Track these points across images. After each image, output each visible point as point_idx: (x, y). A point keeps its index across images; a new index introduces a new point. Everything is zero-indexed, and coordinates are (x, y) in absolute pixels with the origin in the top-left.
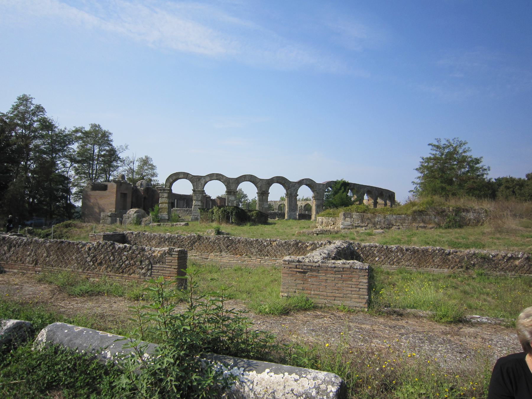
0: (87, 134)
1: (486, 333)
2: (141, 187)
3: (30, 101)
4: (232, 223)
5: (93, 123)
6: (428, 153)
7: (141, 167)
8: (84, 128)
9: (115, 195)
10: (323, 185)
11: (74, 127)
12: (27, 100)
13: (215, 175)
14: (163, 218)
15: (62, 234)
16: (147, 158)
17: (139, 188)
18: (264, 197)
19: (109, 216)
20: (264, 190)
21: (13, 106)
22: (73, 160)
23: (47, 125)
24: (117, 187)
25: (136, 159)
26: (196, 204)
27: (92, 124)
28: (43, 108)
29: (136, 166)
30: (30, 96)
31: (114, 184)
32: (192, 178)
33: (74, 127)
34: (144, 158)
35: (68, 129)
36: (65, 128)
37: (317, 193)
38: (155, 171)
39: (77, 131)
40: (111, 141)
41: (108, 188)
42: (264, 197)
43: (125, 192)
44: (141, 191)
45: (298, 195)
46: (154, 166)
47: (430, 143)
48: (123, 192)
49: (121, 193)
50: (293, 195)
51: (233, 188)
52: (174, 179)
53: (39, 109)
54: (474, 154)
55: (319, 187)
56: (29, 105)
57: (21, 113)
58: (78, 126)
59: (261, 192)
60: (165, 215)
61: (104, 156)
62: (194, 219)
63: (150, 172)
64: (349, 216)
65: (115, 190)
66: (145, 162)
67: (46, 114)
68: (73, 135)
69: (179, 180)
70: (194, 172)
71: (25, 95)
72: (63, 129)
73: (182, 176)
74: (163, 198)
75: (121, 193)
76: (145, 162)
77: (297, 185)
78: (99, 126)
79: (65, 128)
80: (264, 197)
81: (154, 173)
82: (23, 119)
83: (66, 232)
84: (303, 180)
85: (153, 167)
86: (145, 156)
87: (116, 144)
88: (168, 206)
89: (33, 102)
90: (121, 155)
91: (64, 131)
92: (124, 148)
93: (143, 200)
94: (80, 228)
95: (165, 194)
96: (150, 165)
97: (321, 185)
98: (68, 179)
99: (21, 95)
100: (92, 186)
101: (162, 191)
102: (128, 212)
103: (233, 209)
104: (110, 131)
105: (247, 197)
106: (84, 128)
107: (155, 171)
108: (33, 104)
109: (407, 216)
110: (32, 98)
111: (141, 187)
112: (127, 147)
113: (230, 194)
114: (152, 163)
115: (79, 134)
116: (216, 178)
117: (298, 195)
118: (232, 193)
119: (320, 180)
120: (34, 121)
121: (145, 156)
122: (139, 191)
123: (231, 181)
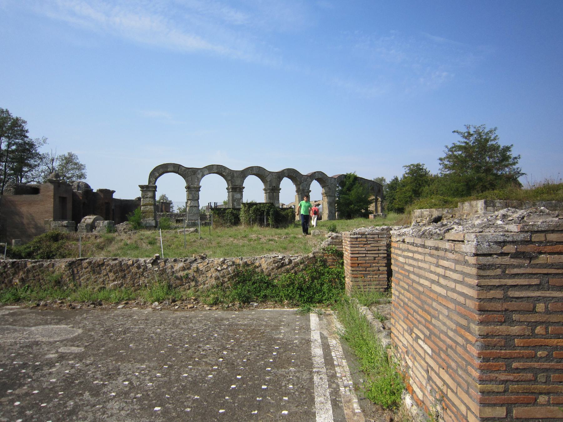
2: (78, 190)
4: (268, 225)
6: (459, 140)
7: (62, 166)
9: (52, 200)
10: (297, 185)
13: (215, 167)
14: (148, 225)
15: (51, 252)
16: (71, 155)
18: (274, 194)
20: (274, 185)
24: (54, 189)
25: (56, 157)
29: (56, 164)
34: (67, 155)
37: (330, 189)
38: (83, 171)
40: (27, 131)
41: (41, 191)
42: (274, 194)
43: (64, 196)
44: (78, 195)
45: (310, 191)
47: (455, 130)
48: (62, 196)
49: (60, 197)
50: (306, 191)
54: (502, 143)
55: (331, 181)
60: (151, 221)
62: (190, 224)
63: (78, 172)
64: (492, 205)
65: (51, 193)
69: (165, 175)
70: (187, 164)
74: (147, 198)
75: (60, 197)
77: (309, 179)
78: (7, 111)
81: (82, 175)
83: (58, 248)
84: (315, 172)
85: (80, 167)
86: (69, 153)
87: (32, 135)
88: (154, 209)
90: (41, 150)
92: (42, 142)
94: (78, 240)
95: (149, 193)
96: (76, 164)
97: (333, 179)
101: (145, 189)
102: (83, 220)
103: (269, 207)
104: (24, 118)
105: (172, 203)
107: (83, 171)
109: (558, 201)
111: (78, 190)
112: (45, 141)
113: (236, 191)
114: (78, 161)
116: (216, 171)
117: (310, 191)
118: (238, 190)
119: (331, 172)
121: (69, 153)
123: (235, 175)
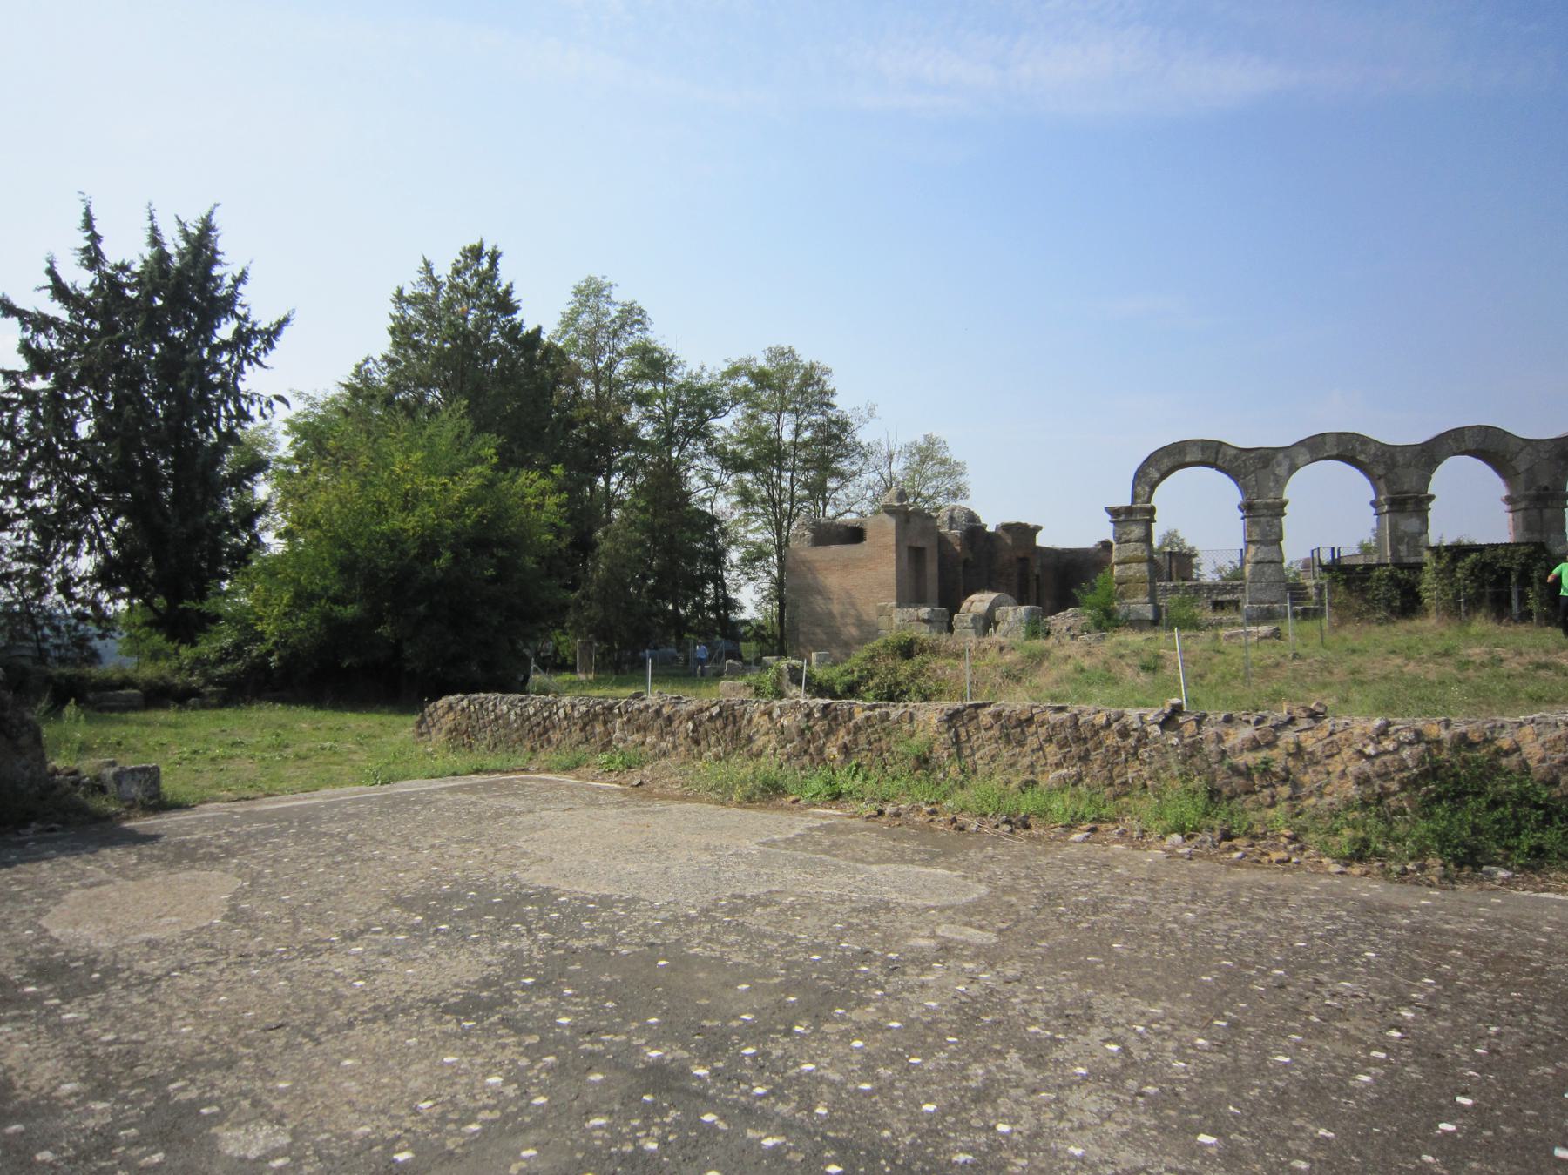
0: (761, 378)
1: (424, 812)
2: (951, 528)
3: (605, 293)
4: (1526, 616)
5: (773, 345)
7: (916, 470)
8: (754, 360)
9: (893, 556)
11: (726, 361)
12: (598, 293)
16: (931, 441)
17: (944, 530)
19: (924, 621)
20: (1544, 482)
21: (563, 314)
22: (734, 463)
23: (654, 364)
26: (1260, 556)
27: (770, 349)
28: (641, 311)
30: (606, 281)
31: (885, 517)
32: (1236, 457)
33: (726, 361)
34: (921, 442)
35: (709, 369)
36: (702, 368)
38: (961, 480)
39: (734, 372)
41: (868, 535)
43: (920, 544)
46: (957, 464)
48: (914, 545)
49: (910, 548)
51: (1409, 483)
52: (1164, 468)
53: (632, 316)
56: (604, 306)
57: (586, 333)
58: (736, 358)
59: (1532, 492)
60: (1140, 606)
61: (806, 444)
63: (948, 484)
65: (891, 539)
66: (927, 454)
67: (651, 328)
68: (725, 385)
69: (1213, 471)
70: (1242, 436)
71: (592, 279)
72: (696, 370)
73: (1166, 463)
74: (1128, 541)
75: (910, 548)
76: (927, 454)
78: (791, 351)
79: (702, 368)
80: (1548, 513)
82: (593, 353)
85: (951, 469)
86: (926, 436)
87: (844, 403)
89: (614, 298)
91: (698, 377)
92: (865, 415)
93: (960, 569)
96: (943, 462)
98: (713, 520)
99: (579, 280)
100: (812, 531)
102: (965, 605)
103: (1528, 556)
106: (754, 360)
107: (961, 480)
108: (615, 304)
110: (611, 286)
111: (951, 528)
112: (871, 415)
113: (1403, 511)
114: (947, 455)
115: (743, 381)
116: (1335, 452)
118: (1410, 506)
120: (620, 355)
121: (926, 436)
122: (948, 543)
123: (1400, 459)
